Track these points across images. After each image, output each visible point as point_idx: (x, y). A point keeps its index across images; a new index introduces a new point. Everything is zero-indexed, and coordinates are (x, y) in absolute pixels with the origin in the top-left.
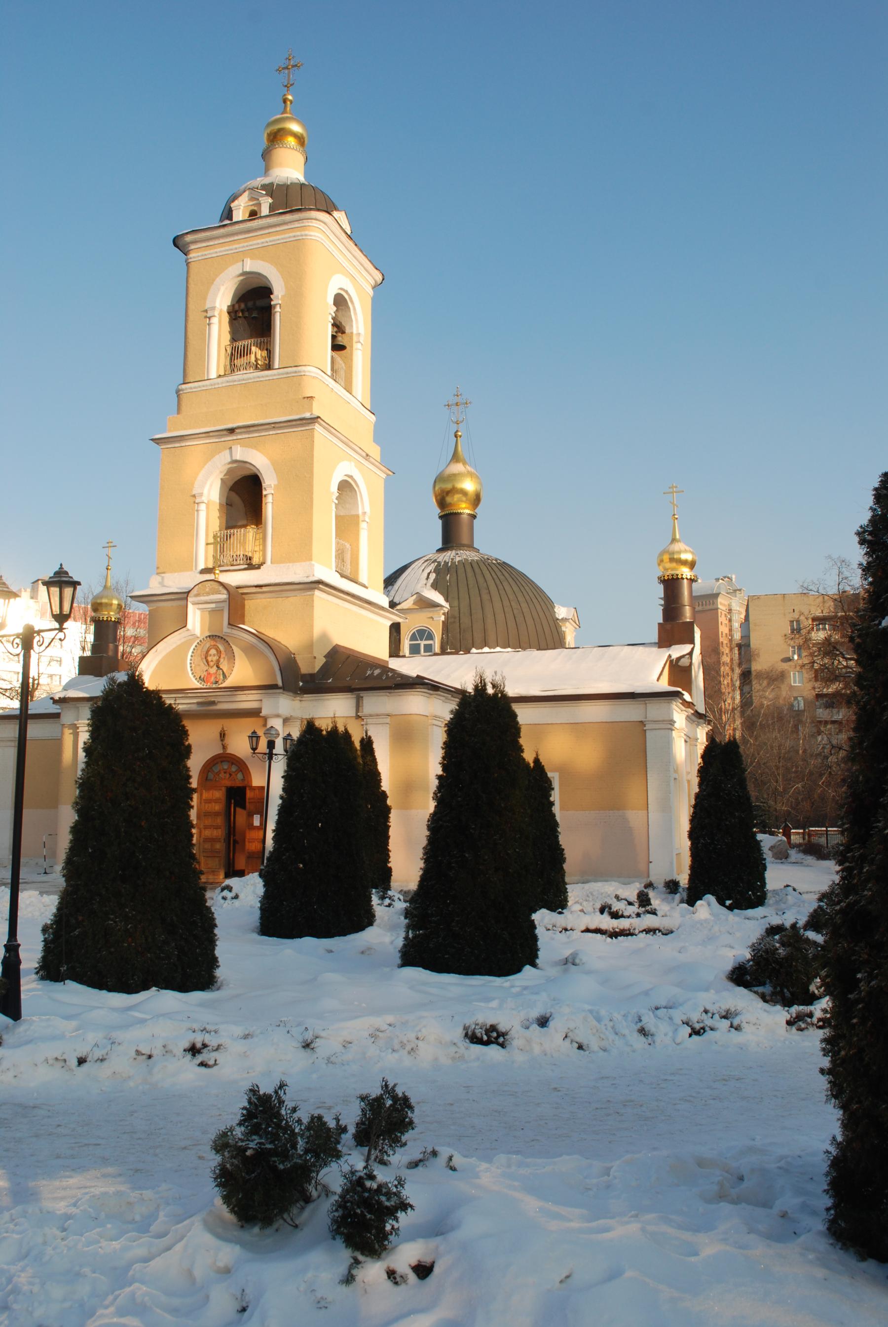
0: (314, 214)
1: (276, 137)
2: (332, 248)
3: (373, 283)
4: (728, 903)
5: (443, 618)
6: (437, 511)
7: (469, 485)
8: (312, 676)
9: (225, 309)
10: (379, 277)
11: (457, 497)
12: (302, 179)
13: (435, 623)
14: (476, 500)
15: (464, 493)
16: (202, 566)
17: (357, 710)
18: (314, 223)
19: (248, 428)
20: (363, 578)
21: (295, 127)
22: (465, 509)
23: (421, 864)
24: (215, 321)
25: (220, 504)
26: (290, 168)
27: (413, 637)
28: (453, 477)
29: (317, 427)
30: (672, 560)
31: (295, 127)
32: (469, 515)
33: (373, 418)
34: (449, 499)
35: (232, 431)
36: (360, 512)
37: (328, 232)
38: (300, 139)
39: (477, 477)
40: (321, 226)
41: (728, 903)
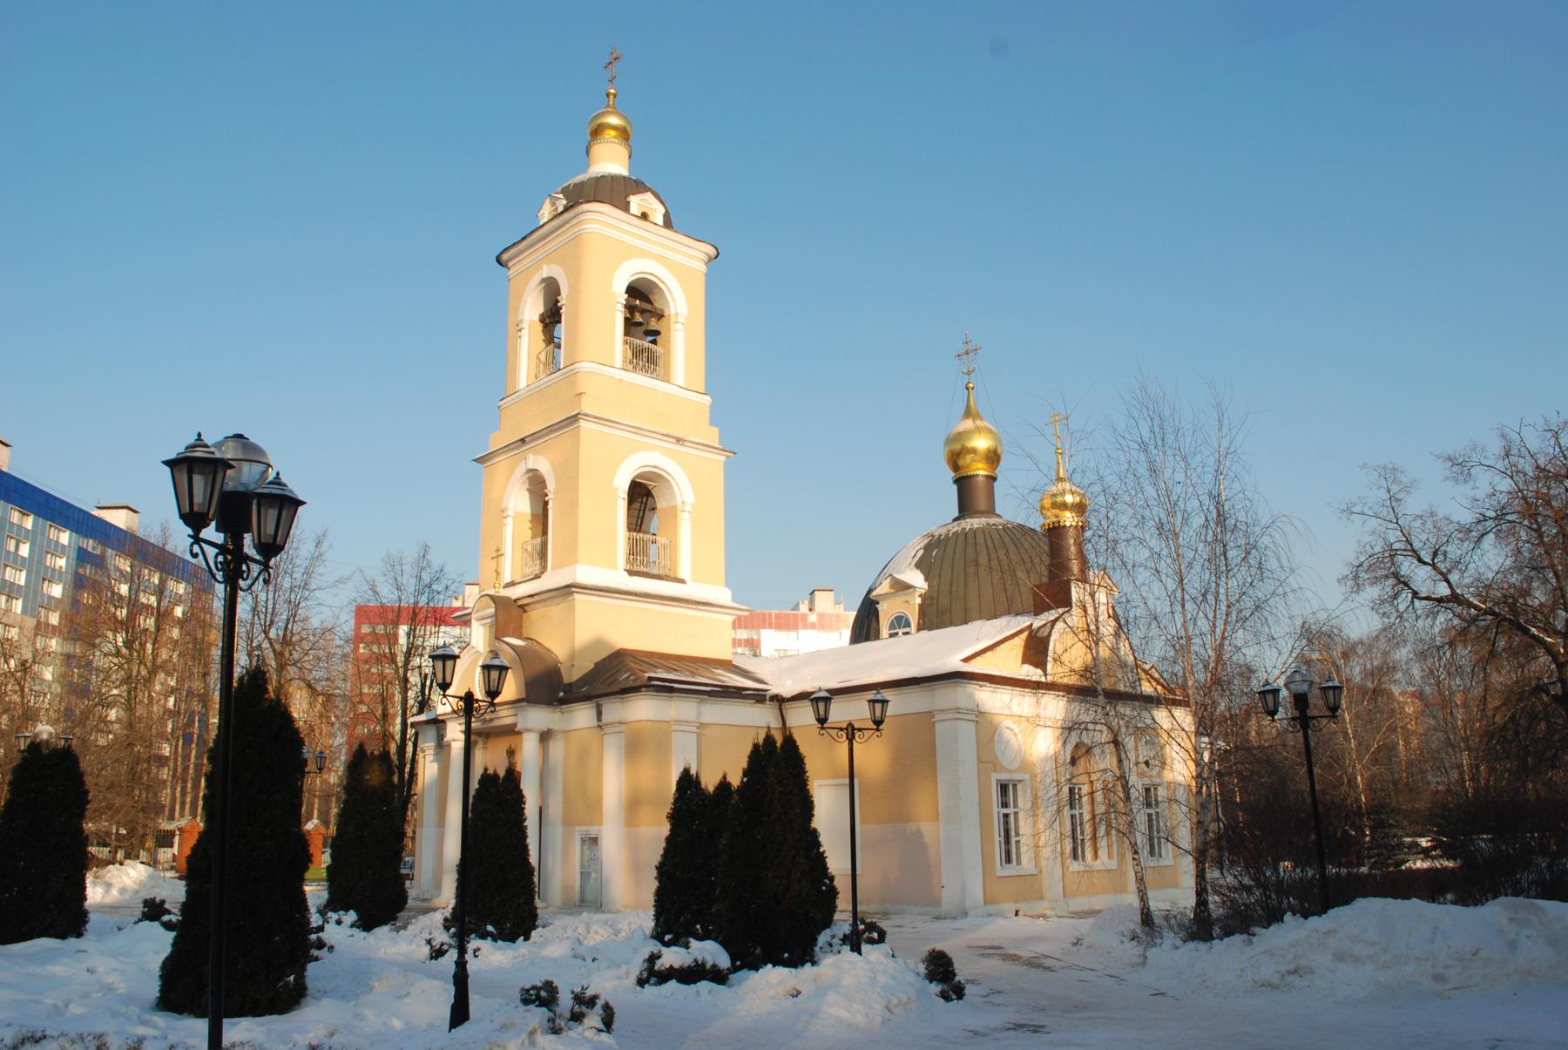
0: (586, 207)
1: (597, 132)
2: (616, 234)
3: (706, 258)
4: (667, 937)
5: (919, 600)
6: (950, 475)
7: (981, 443)
8: (571, 684)
9: (536, 318)
10: (712, 252)
11: (969, 457)
12: (625, 173)
13: (911, 607)
14: (993, 458)
15: (974, 451)
16: (508, 580)
17: (599, 719)
18: (589, 216)
19: (535, 436)
20: (684, 571)
21: (614, 120)
22: (981, 470)
23: (657, 884)
24: (525, 333)
25: (533, 515)
26: (610, 160)
27: (892, 626)
28: (960, 436)
29: (582, 423)
30: (1055, 505)
31: (614, 120)
32: (988, 477)
33: (707, 400)
34: (961, 463)
35: (523, 440)
36: (679, 502)
37: (610, 221)
38: (624, 134)
39: (991, 432)
40: (598, 217)
41: (667, 937)
